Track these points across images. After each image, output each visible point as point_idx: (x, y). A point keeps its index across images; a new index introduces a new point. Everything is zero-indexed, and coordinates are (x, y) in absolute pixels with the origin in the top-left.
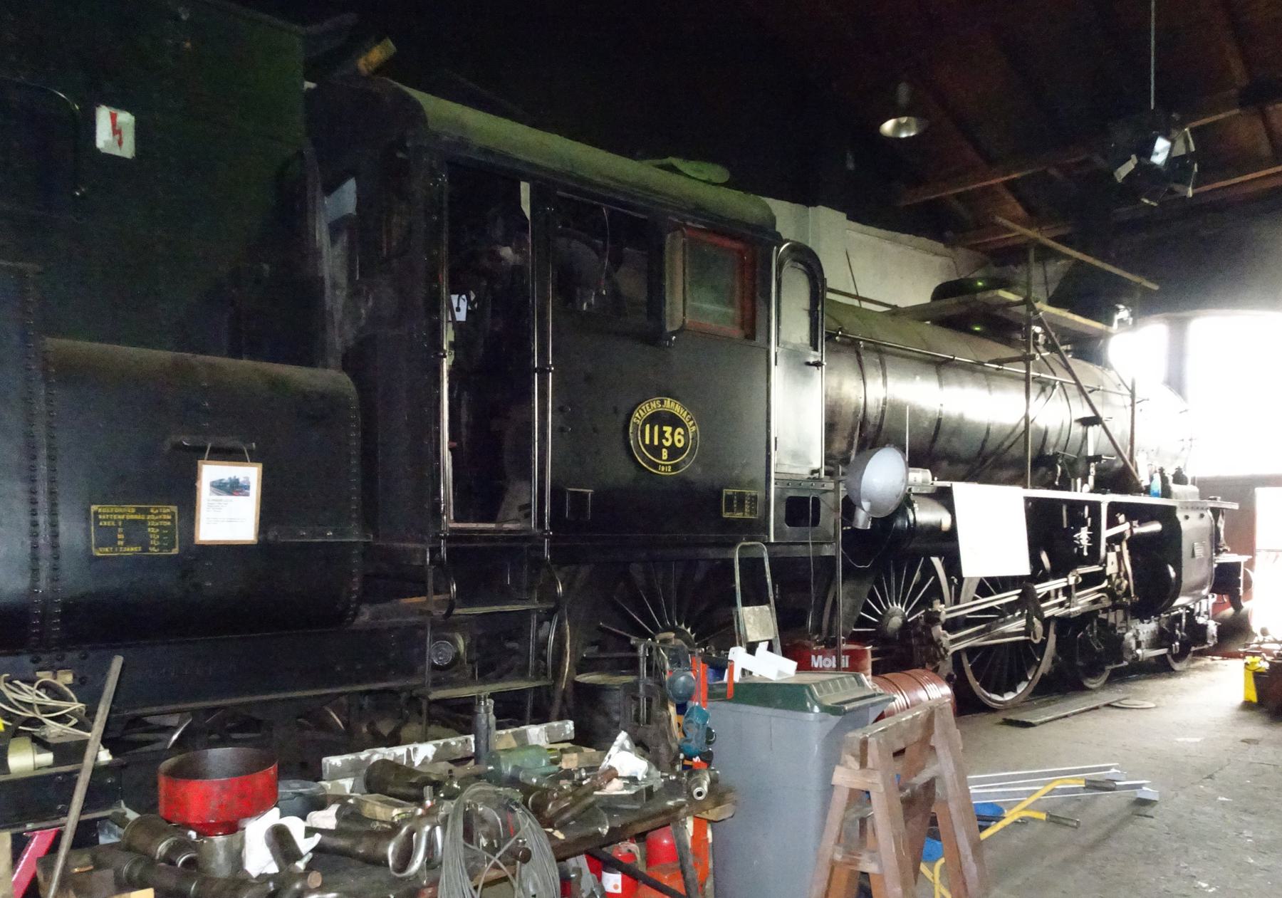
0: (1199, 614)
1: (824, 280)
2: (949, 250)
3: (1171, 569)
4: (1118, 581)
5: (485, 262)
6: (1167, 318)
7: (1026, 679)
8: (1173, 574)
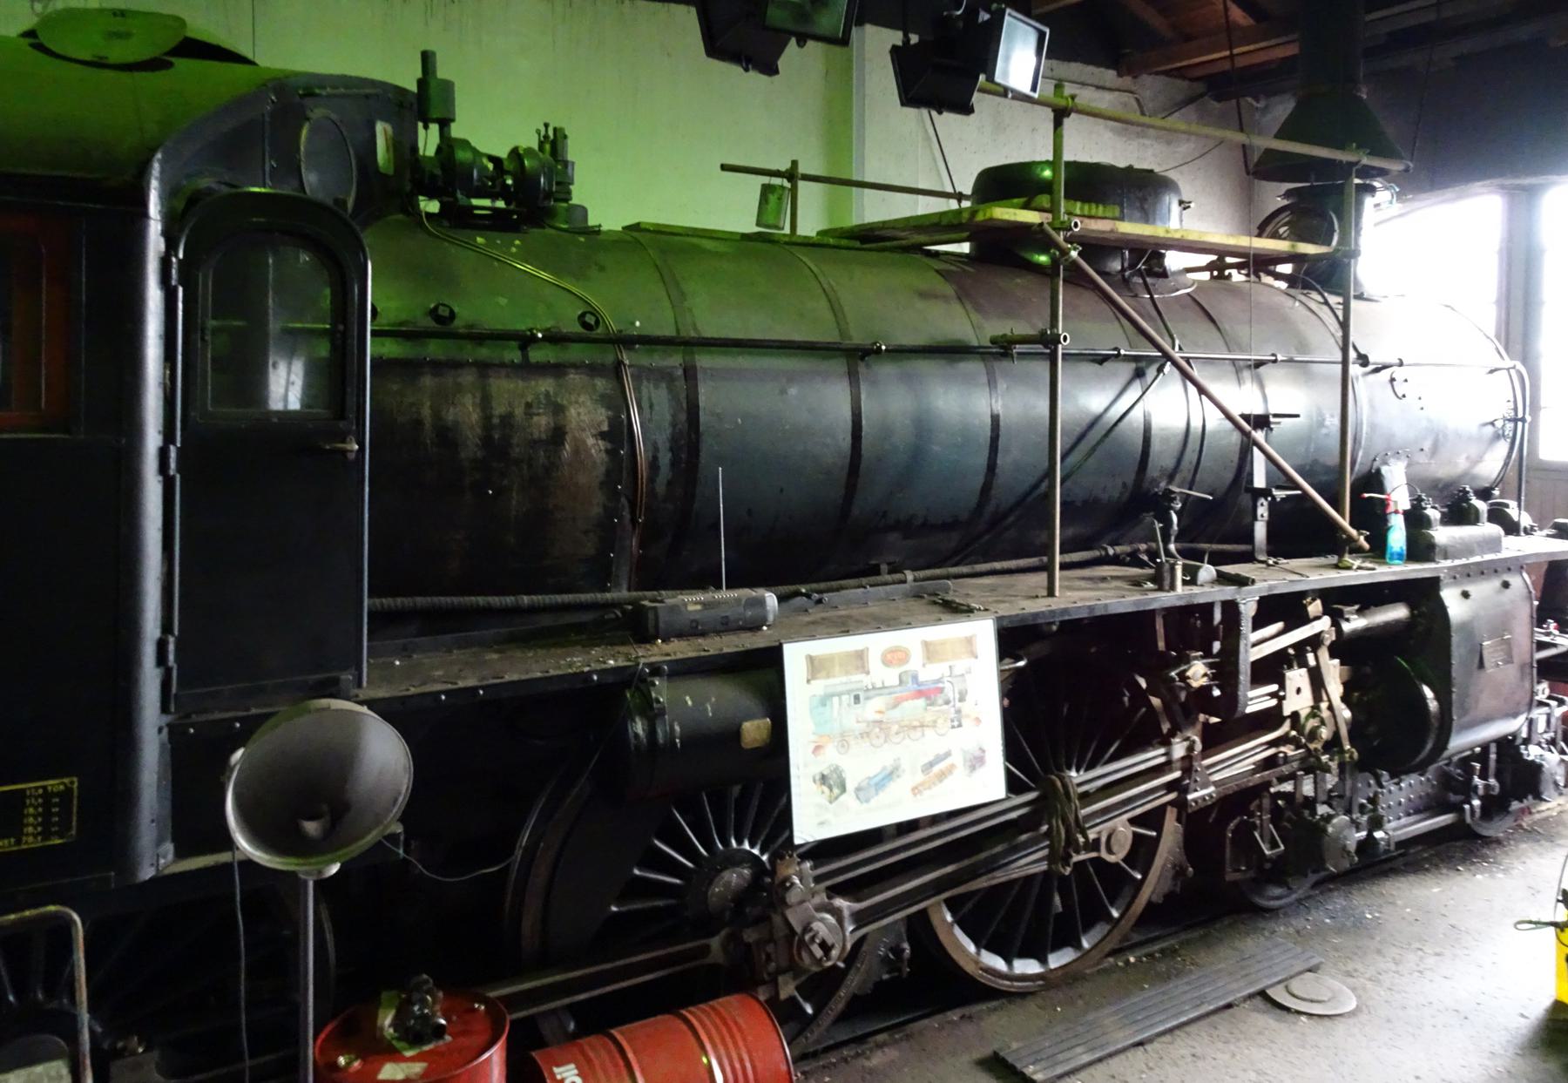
0: (1527, 741)
1: (434, 72)
2: (1127, 81)
3: (1428, 692)
4: (1312, 723)
5: (547, 156)
6: (1502, 187)
7: (1077, 945)
8: (1433, 705)
